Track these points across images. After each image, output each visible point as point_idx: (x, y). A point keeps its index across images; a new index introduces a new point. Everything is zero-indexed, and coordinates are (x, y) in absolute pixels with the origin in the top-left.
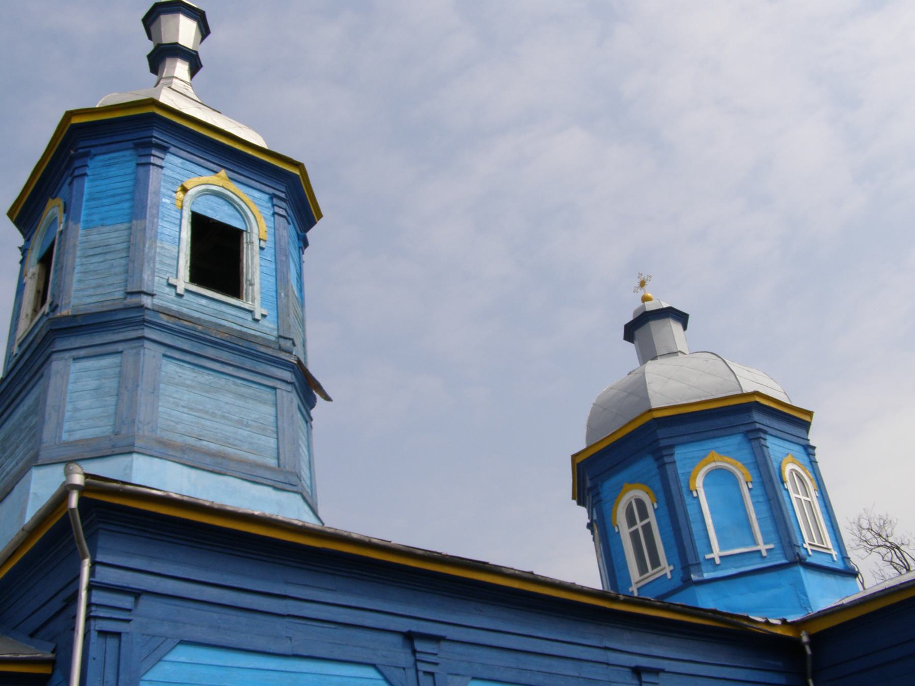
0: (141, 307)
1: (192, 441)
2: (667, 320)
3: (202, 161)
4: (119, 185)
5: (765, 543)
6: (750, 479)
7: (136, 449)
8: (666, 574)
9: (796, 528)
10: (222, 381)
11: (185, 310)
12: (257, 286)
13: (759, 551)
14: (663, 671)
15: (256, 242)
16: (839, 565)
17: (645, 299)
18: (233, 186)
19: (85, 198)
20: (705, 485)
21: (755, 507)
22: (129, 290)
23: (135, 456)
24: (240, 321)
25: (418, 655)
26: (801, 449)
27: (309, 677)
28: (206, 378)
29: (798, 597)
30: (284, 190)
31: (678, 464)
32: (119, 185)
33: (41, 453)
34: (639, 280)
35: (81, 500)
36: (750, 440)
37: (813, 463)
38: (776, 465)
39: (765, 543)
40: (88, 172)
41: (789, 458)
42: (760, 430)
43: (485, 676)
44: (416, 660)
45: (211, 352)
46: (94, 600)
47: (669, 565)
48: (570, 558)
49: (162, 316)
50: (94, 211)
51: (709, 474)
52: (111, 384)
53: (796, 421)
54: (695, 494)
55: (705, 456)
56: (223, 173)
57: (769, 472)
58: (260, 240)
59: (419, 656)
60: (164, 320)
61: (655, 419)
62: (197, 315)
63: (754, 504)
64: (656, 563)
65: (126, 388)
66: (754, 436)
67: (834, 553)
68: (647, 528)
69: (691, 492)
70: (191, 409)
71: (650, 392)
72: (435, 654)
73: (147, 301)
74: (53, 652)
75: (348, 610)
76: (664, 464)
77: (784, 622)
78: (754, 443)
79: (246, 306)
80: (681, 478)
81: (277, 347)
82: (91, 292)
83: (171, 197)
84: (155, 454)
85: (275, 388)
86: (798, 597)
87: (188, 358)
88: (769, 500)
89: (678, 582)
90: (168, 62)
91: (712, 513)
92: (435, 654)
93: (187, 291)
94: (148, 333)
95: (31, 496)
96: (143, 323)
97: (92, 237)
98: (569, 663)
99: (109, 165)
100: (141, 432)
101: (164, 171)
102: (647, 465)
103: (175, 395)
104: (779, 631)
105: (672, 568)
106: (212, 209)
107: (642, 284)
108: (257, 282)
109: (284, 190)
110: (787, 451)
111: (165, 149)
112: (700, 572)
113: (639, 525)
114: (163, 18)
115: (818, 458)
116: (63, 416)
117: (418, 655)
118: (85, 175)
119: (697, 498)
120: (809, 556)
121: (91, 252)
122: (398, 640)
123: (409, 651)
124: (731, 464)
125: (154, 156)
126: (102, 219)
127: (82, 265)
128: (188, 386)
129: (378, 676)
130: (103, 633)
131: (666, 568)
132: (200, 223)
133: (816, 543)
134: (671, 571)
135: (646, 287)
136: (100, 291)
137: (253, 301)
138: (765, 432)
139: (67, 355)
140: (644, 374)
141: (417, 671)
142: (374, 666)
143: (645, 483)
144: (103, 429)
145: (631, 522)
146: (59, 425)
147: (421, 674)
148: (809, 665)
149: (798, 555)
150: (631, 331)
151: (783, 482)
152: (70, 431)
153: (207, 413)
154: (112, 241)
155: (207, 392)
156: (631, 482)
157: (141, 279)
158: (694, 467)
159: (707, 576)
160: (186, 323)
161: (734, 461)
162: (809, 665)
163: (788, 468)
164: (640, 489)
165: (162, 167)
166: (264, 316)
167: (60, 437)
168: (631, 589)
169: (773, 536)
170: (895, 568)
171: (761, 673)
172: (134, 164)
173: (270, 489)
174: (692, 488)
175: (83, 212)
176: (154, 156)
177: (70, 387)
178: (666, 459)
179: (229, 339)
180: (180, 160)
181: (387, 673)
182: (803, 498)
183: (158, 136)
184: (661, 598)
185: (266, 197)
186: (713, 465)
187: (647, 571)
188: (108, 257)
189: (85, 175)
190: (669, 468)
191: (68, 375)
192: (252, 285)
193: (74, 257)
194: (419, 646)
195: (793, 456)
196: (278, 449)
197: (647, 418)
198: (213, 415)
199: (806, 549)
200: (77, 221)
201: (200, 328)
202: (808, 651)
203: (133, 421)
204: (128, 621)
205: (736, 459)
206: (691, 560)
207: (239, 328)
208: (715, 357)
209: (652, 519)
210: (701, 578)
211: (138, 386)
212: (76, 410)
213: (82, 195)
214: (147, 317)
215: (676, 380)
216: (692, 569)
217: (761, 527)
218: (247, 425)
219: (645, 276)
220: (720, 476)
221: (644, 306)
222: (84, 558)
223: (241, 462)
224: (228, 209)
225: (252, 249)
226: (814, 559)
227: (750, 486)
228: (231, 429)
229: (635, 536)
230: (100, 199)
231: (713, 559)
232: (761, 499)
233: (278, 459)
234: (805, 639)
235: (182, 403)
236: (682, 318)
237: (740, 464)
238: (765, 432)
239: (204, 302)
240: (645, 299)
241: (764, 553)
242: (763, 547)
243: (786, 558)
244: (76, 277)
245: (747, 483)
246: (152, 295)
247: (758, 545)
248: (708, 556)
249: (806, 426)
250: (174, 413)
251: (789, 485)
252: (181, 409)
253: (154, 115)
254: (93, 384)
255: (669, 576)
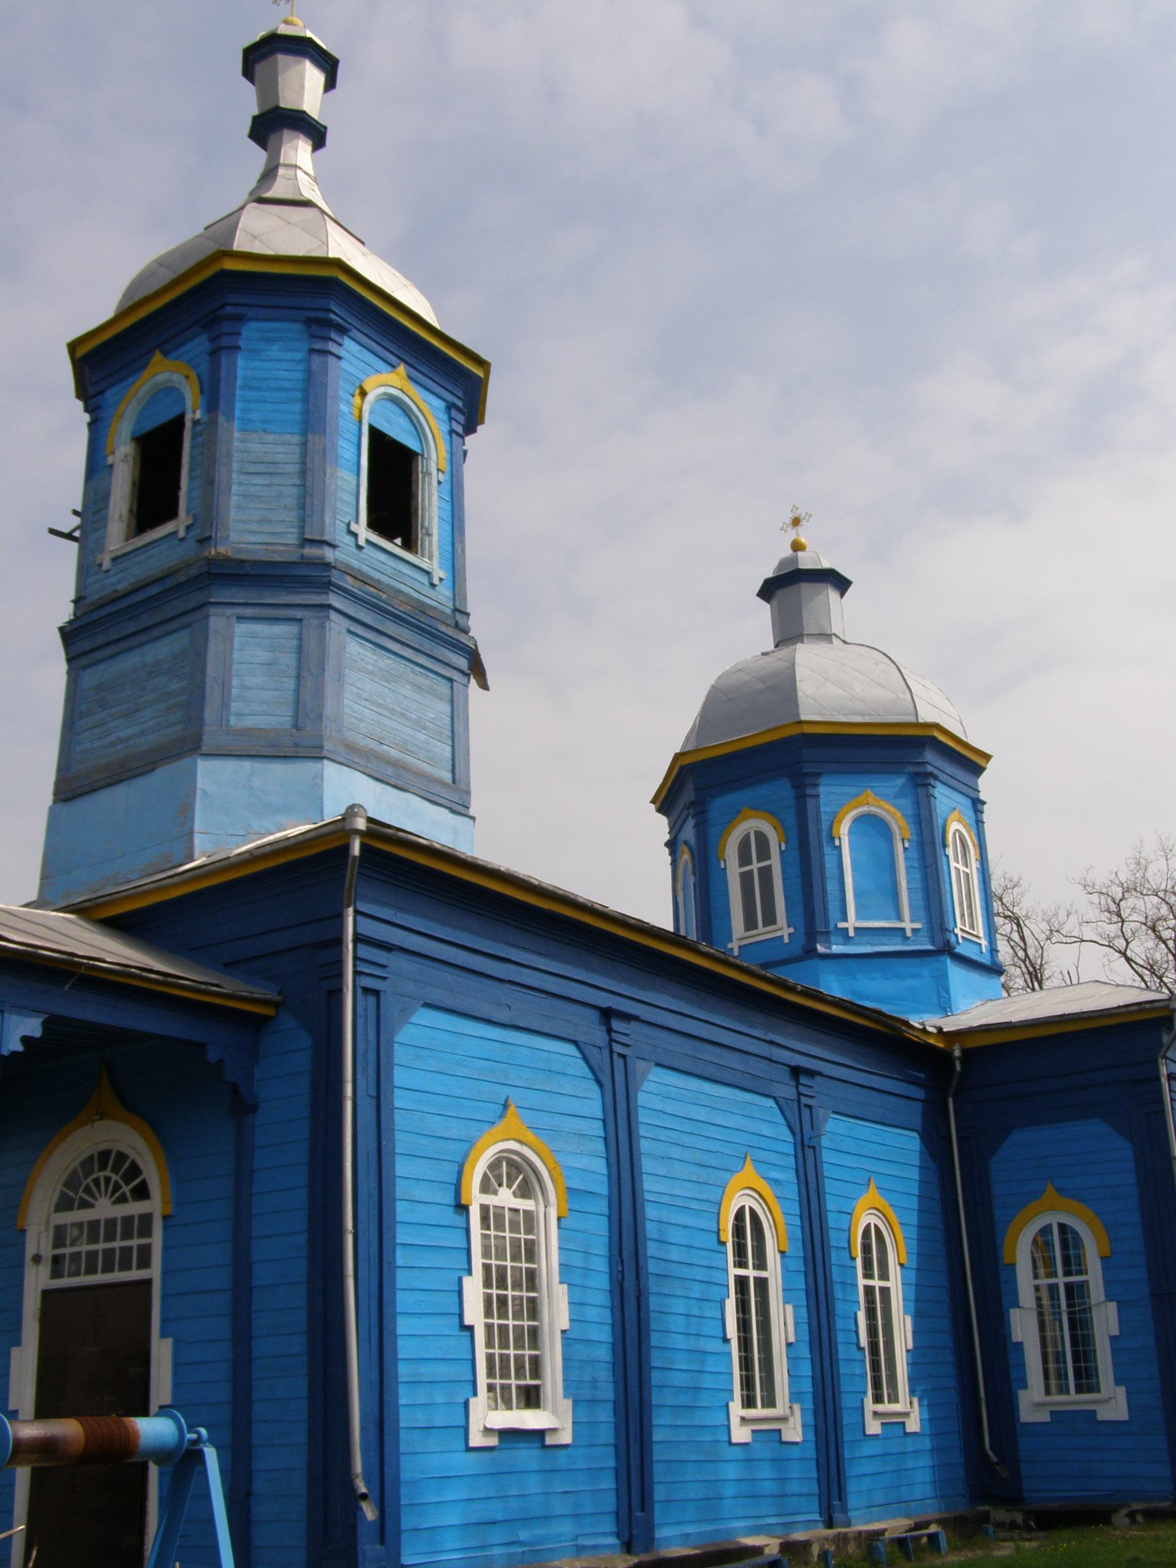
0: (327, 566)
1: (373, 745)
2: (824, 585)
3: (380, 348)
4: (286, 375)
5: (912, 921)
6: (908, 835)
7: (325, 753)
8: (782, 937)
9: (950, 908)
10: (402, 667)
11: (365, 569)
12: (435, 539)
13: (903, 930)
14: (820, 1074)
15: (434, 471)
16: (985, 959)
17: (797, 546)
18: (413, 389)
19: (239, 383)
20: (851, 832)
21: (907, 873)
22: (308, 536)
23: (326, 762)
24: (418, 586)
25: (613, 1034)
26: (968, 803)
27: (523, 1050)
28: (387, 662)
29: (939, 993)
30: (460, 394)
31: (822, 799)
32: (286, 375)
33: (205, 738)
34: (792, 516)
35: (363, 847)
36: (917, 785)
37: (979, 823)
38: (940, 822)
39: (912, 921)
40: (241, 343)
41: (955, 814)
42: (931, 775)
43: (666, 1063)
44: (611, 1040)
45: (391, 628)
46: (360, 954)
47: (789, 926)
48: (636, 881)
49: (348, 577)
50: (253, 406)
51: (857, 820)
52: (288, 660)
53: (970, 763)
54: (837, 843)
55: (857, 796)
56: (402, 369)
57: (932, 832)
58: (438, 470)
59: (802, 1089)
60: (349, 583)
61: (803, 734)
62: (376, 575)
63: (907, 868)
64: (770, 919)
65: (309, 670)
66: (921, 782)
67: (984, 943)
68: (766, 873)
69: (833, 839)
70: (373, 703)
71: (800, 693)
72: (627, 1035)
73: (329, 555)
74: (279, 993)
75: (557, 979)
76: (805, 796)
77: (940, 1030)
78: (921, 791)
79: (424, 566)
80: (824, 817)
81: (452, 623)
82: (255, 527)
83: (349, 404)
84: (341, 760)
85: (451, 680)
86: (939, 993)
87: (370, 635)
88: (926, 867)
89: (797, 950)
90: (287, 134)
91: (854, 870)
92: (627, 1035)
93: (368, 542)
94: (334, 600)
95: (199, 793)
96: (327, 586)
97: (253, 446)
98: (737, 1055)
99: (269, 341)
100: (328, 732)
101: (343, 364)
102: (781, 790)
103: (358, 685)
104: (932, 1041)
105: (792, 930)
106: (388, 421)
107: (796, 522)
108: (435, 531)
109: (461, 395)
110: (954, 805)
111: (343, 331)
112: (828, 944)
113: (755, 866)
114: (282, 58)
115: (986, 817)
116: (230, 693)
117: (801, 1088)
118: (238, 348)
119: (839, 848)
120: (958, 943)
121: (252, 469)
122: (595, 1015)
123: (604, 1028)
124: (889, 812)
125: (333, 340)
126: (265, 422)
127: (240, 484)
128: (370, 673)
129: (579, 1055)
130: (367, 990)
131: (783, 929)
132: (381, 444)
133: (967, 929)
134: (790, 934)
135: (800, 529)
136: (267, 528)
137: (431, 558)
138: (936, 778)
139: (229, 611)
140: (794, 664)
141: (611, 1052)
142: (575, 1043)
143: (773, 814)
144: (281, 718)
145: (744, 859)
146: (225, 704)
147: (615, 1056)
148: (955, 1082)
149: (948, 941)
150: (768, 590)
151: (945, 846)
152: (239, 715)
153: (387, 708)
154: (279, 458)
155: (387, 681)
156: (755, 808)
157: (323, 525)
158: (841, 806)
159: (836, 949)
160: (371, 589)
161: (892, 809)
162: (955, 1082)
163: (954, 826)
164: (759, 818)
165: (339, 358)
166: (441, 580)
167: (228, 721)
168: (729, 946)
169: (922, 913)
170: (1012, 947)
171: (905, 1084)
172: (305, 346)
173: (446, 811)
174: (834, 833)
175: (238, 405)
176: (333, 340)
177: (236, 655)
178: (809, 791)
179: (411, 613)
180: (358, 347)
181: (587, 1052)
182: (962, 868)
183: (338, 312)
184: (765, 966)
185: (441, 405)
186: (864, 809)
187: (756, 927)
188: (276, 480)
189: (238, 348)
190: (810, 803)
191: (232, 638)
192: (429, 535)
193: (230, 472)
194: (616, 1025)
195: (960, 812)
196: (453, 759)
197: (794, 731)
198: (393, 711)
199: (956, 935)
200: (230, 418)
201: (384, 596)
202: (958, 1067)
203: (320, 717)
204: (384, 978)
205: (895, 806)
206: (820, 928)
207: (416, 595)
208: (888, 661)
209: (775, 862)
210: (828, 951)
211: (323, 670)
212: (244, 687)
213: (235, 378)
214: (333, 580)
215: (834, 685)
216: (818, 938)
217: (910, 899)
218: (425, 728)
219: (801, 512)
220: (871, 824)
221: (795, 560)
222: (348, 906)
223: (420, 775)
224: (402, 420)
225: (430, 483)
226: (963, 949)
227: (907, 845)
228: (409, 731)
229: (746, 879)
230: (258, 389)
231: (846, 929)
232: (916, 864)
233: (453, 772)
234: (957, 1053)
235: (365, 695)
236: (841, 584)
237: (899, 815)
238: (936, 778)
239: (383, 557)
240: (797, 546)
241: (909, 933)
242: (908, 925)
243: (933, 943)
244: (234, 500)
245: (903, 840)
246: (334, 546)
247: (903, 921)
248: (841, 925)
249: (978, 770)
250: (357, 707)
251: (950, 851)
252: (364, 703)
253: (335, 282)
254: (263, 656)
255: (786, 940)
